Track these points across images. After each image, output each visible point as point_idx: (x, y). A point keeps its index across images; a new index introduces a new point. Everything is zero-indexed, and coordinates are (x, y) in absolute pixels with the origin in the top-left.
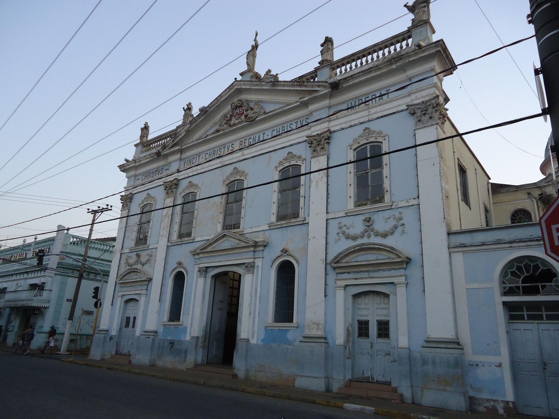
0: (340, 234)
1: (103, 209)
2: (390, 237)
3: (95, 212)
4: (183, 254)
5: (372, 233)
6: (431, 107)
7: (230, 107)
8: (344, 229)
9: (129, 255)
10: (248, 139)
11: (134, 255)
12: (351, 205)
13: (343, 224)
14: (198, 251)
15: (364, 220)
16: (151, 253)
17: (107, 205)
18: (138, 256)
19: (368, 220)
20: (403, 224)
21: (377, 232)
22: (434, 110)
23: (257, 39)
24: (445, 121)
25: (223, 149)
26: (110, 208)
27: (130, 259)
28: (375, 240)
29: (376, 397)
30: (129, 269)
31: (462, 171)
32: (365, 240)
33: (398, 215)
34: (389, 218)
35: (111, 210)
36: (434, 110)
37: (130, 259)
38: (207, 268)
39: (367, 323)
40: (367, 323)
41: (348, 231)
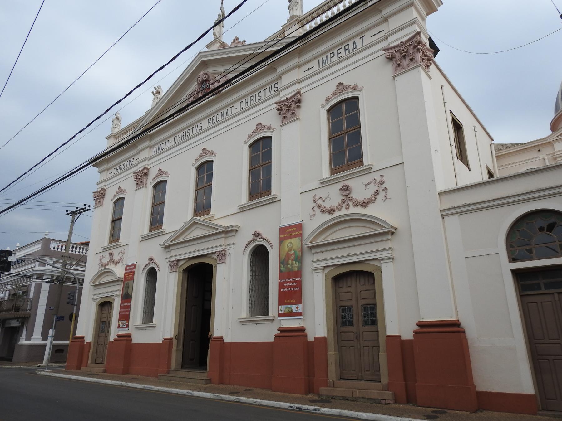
0: (316, 209)
1: (81, 209)
2: (371, 206)
3: (74, 213)
4: (154, 250)
5: (351, 204)
6: (412, 47)
7: (196, 83)
8: (320, 202)
9: (102, 254)
10: (216, 115)
11: (106, 254)
12: (326, 174)
13: (317, 197)
14: (168, 243)
15: (341, 189)
16: (123, 250)
17: (85, 205)
18: (111, 255)
19: (346, 189)
20: (386, 189)
21: (357, 201)
22: (415, 50)
23: (223, 6)
24: (431, 64)
25: (191, 130)
26: (88, 208)
27: (103, 259)
28: (353, 210)
29: (363, 398)
30: (102, 270)
31: (457, 127)
32: (344, 212)
33: (379, 179)
34: (369, 184)
35: (89, 210)
36: (415, 50)
37: (103, 259)
38: (178, 261)
39: (350, 309)
40: (350, 309)
41: (323, 204)
